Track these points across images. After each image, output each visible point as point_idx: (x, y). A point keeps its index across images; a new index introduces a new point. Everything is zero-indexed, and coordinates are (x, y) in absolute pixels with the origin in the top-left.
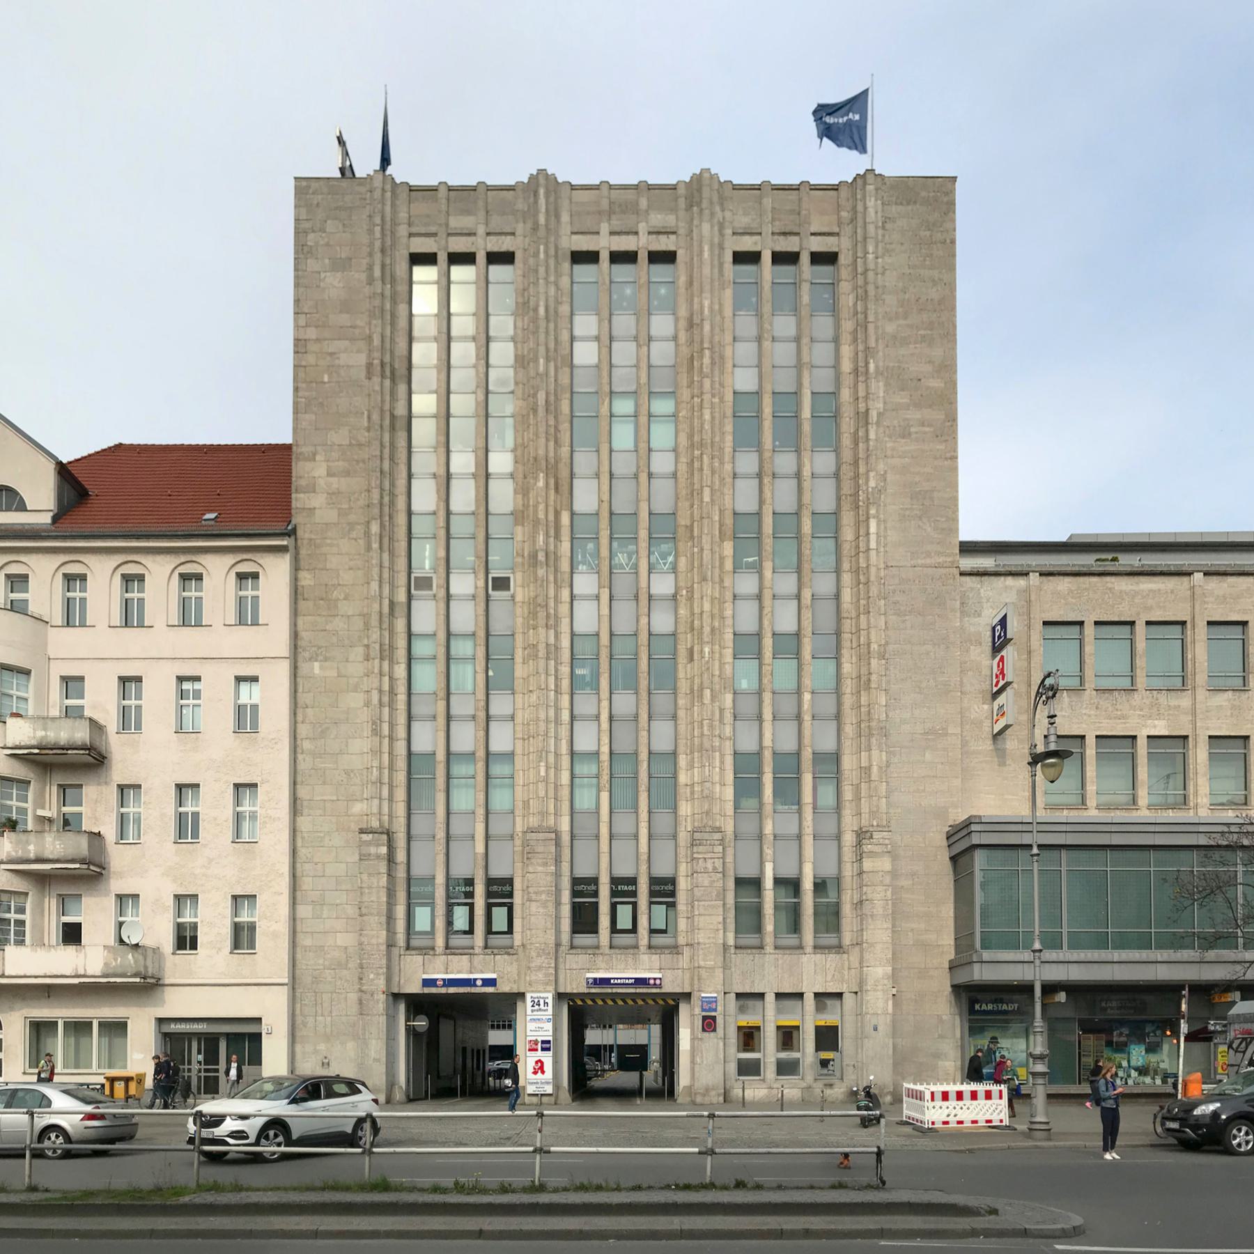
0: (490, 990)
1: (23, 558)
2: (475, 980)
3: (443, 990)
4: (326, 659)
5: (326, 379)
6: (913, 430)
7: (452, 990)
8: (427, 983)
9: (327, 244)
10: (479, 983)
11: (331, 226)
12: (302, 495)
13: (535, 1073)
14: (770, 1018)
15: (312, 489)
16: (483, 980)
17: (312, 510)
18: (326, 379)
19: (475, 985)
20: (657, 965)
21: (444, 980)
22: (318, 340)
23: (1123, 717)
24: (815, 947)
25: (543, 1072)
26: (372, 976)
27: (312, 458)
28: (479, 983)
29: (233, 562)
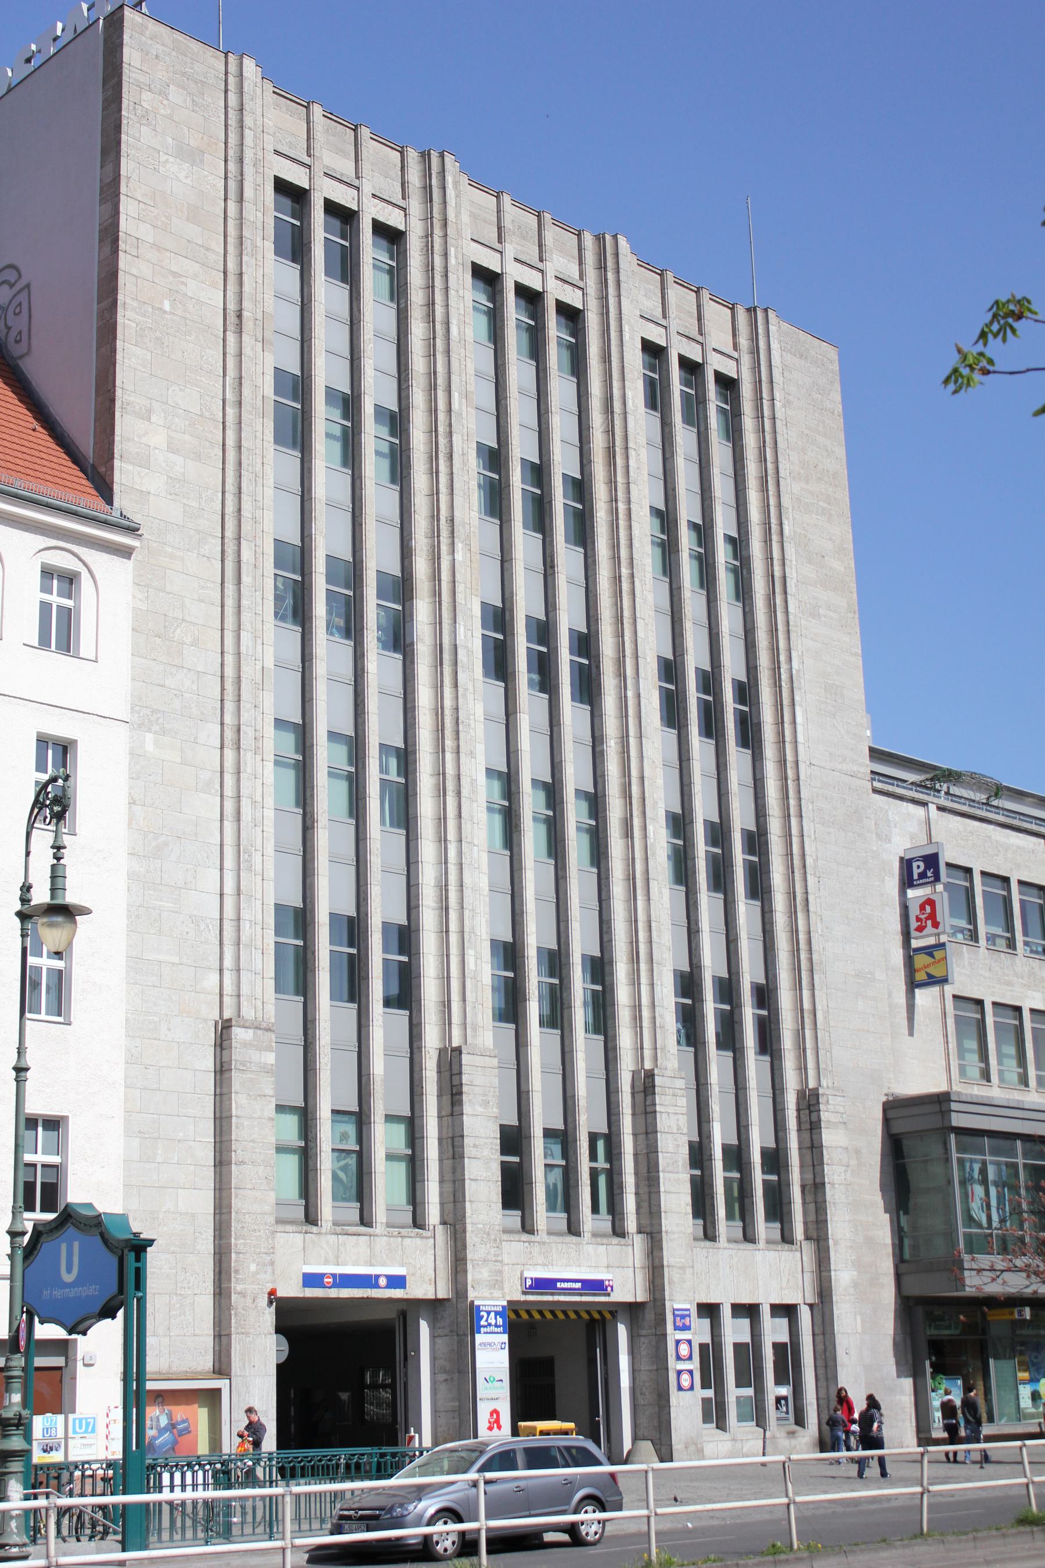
0: (397, 1293)
1: (81, 551)
2: (377, 1277)
3: (333, 1293)
4: (164, 732)
5: (167, 306)
6: (821, 611)
7: (346, 1293)
8: (311, 1280)
9: (170, 117)
10: (383, 1282)
11: (175, 95)
12: (130, 467)
13: (490, 1429)
14: (735, 1331)
15: (145, 462)
16: (388, 1277)
17: (145, 494)
18: (167, 306)
19: (377, 1286)
20: (604, 1262)
21: (334, 1276)
22: (156, 247)
23: (1009, 984)
24: (335, 1224)
25: (499, 1427)
26: (253, 1267)
27: (146, 415)
28: (383, 1282)
29: (44, 546)
